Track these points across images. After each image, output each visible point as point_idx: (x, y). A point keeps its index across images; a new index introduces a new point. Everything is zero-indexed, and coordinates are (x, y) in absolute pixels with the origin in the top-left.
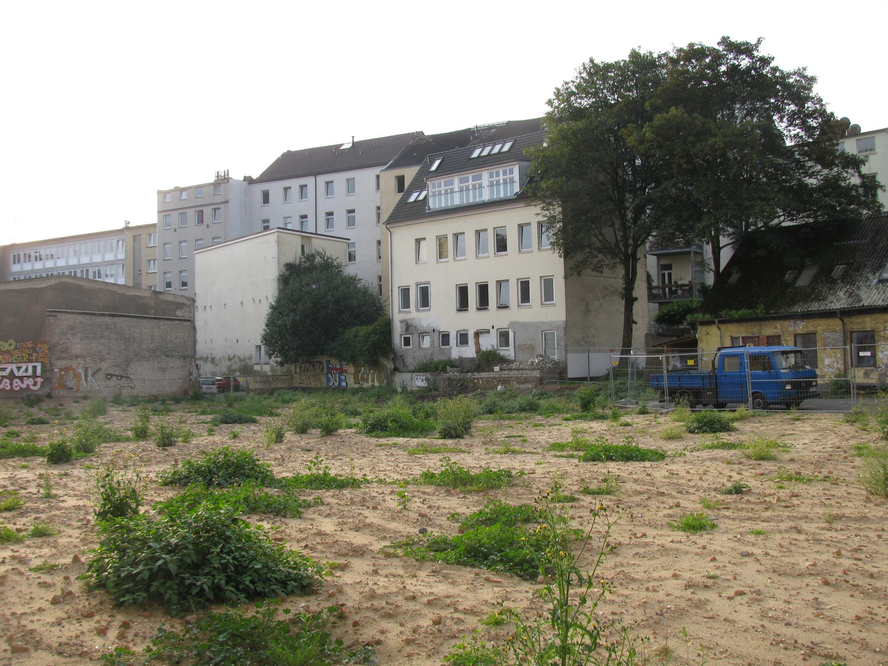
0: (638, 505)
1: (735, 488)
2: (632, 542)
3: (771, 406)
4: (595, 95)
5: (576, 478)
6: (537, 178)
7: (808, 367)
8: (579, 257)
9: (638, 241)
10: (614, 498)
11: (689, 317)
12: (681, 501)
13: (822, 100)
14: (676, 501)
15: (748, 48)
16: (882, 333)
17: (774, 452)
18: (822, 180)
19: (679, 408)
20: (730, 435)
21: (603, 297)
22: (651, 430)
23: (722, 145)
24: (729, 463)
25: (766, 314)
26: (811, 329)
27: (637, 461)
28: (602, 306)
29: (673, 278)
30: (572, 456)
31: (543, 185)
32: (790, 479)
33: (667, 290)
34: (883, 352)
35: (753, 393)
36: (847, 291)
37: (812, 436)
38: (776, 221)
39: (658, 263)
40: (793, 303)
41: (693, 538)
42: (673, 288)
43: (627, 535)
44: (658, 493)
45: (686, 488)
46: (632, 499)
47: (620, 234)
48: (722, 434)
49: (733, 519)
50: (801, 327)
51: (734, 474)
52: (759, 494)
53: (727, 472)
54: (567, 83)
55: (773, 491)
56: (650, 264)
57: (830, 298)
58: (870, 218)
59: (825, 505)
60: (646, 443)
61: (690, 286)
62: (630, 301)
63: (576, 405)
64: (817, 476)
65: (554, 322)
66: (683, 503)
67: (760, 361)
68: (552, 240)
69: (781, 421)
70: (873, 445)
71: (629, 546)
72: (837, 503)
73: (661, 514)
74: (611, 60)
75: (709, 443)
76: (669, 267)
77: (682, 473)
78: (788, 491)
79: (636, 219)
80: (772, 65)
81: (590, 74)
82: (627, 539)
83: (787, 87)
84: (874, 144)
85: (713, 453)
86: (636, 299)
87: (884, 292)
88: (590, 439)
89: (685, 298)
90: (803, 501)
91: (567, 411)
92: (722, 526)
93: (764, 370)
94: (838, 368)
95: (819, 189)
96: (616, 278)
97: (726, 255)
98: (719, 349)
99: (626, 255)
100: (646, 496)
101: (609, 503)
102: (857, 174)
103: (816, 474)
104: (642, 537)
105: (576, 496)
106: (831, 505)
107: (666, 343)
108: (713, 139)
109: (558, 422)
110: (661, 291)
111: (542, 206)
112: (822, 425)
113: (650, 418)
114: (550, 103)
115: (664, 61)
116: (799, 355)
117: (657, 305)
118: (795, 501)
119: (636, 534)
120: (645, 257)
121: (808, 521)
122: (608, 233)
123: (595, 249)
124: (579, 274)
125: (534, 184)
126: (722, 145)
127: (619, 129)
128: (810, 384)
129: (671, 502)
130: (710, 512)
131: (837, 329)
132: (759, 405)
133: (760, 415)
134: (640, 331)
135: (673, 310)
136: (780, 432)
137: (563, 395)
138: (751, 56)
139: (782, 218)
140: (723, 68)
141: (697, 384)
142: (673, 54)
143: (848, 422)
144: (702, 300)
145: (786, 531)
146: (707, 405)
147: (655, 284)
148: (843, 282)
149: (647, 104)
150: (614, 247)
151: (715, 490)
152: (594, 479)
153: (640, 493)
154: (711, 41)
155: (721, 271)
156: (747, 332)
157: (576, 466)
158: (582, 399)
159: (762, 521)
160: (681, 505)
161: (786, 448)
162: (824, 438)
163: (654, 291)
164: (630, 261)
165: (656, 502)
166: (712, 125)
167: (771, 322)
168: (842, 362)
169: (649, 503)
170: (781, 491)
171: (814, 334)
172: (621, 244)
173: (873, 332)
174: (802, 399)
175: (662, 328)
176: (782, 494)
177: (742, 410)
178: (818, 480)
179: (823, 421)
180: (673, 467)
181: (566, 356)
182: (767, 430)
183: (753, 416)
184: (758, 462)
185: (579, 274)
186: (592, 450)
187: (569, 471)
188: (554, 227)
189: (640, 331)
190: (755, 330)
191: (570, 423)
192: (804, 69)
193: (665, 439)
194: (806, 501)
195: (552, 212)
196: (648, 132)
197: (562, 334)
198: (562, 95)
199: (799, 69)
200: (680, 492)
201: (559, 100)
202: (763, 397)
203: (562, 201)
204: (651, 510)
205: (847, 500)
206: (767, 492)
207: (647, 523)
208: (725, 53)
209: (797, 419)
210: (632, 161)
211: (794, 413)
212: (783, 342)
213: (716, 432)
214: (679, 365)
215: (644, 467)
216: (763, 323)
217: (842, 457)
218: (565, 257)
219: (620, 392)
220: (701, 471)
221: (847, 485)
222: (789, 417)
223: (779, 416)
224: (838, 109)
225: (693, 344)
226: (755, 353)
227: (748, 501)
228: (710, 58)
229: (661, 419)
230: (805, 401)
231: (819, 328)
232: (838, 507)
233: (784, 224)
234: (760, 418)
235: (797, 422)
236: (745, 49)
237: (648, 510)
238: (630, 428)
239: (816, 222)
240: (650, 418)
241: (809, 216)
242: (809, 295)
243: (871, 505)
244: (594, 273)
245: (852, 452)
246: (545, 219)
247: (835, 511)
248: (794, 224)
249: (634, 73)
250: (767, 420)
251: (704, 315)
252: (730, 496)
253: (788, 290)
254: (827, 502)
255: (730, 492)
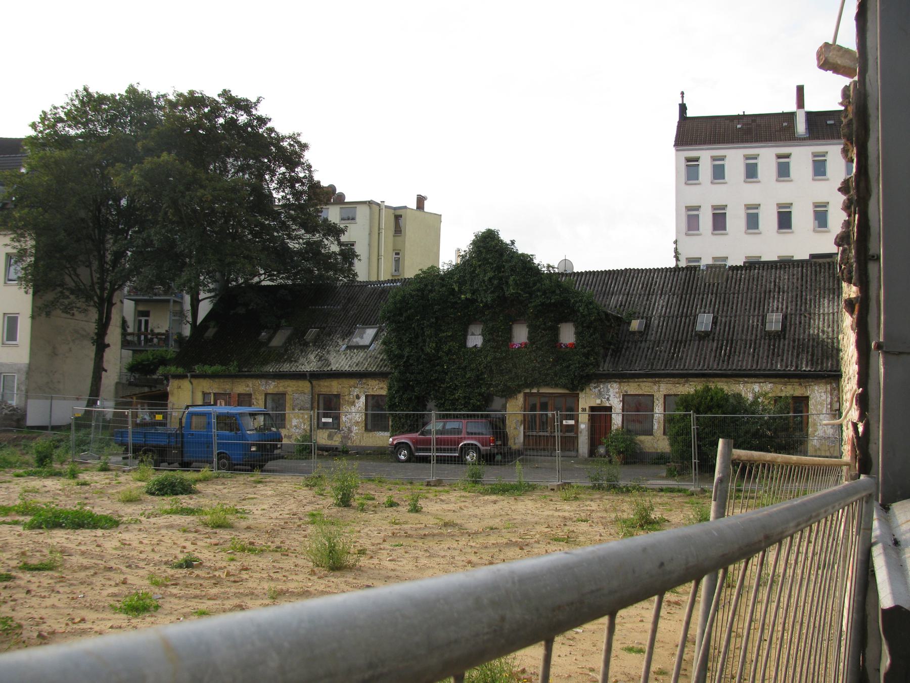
0: (82, 583)
1: (186, 561)
2: (69, 629)
3: (236, 467)
4: (85, 125)
5: (16, 551)
6: (11, 206)
7: (274, 429)
8: (50, 296)
9: (115, 285)
10: (57, 574)
11: (161, 370)
12: (129, 577)
13: (311, 167)
14: (122, 577)
15: (247, 105)
16: (347, 398)
17: (231, 518)
18: (304, 244)
19: (142, 466)
20: (191, 499)
21: (73, 341)
22: (110, 491)
23: (210, 198)
24: (185, 531)
25: (239, 371)
26: (281, 389)
27: (88, 528)
28: (70, 350)
29: (150, 325)
30: (16, 523)
31: (17, 215)
32: (243, 550)
33: (143, 337)
34: (346, 415)
35: (218, 454)
36: (317, 354)
37: (272, 501)
38: (256, 279)
39: (135, 309)
40: (266, 362)
41: (134, 621)
42: (149, 336)
43: (64, 620)
44: (105, 567)
45: (136, 561)
46: (76, 575)
47: (96, 276)
48: (184, 496)
49: (180, 598)
50: (272, 387)
51: (188, 544)
52: (210, 567)
53: (182, 542)
54: (55, 108)
55: (224, 564)
56: (126, 308)
57: (302, 360)
58: (344, 285)
59: (272, 579)
60: (101, 508)
61: (167, 334)
62: (101, 346)
63: (31, 458)
64: (270, 547)
65: (15, 364)
66: (131, 579)
67: (228, 422)
68: (20, 275)
69: (244, 484)
70: (326, 511)
71: (64, 635)
72: (284, 576)
73: (105, 593)
74: (107, 92)
75: (168, 507)
76: (146, 314)
77: (135, 544)
78: (239, 564)
79: (115, 262)
80: (269, 125)
81: (82, 102)
82: (63, 626)
83: (281, 149)
84: (355, 213)
85: (171, 519)
86: (108, 345)
87: (351, 358)
88: (41, 501)
89: (161, 347)
90: (252, 574)
91: (20, 467)
92: (167, 606)
93: (231, 430)
94: (304, 429)
95: (299, 253)
96: (89, 322)
97: (205, 308)
98: (187, 407)
99: (101, 299)
100: (92, 572)
101: (50, 581)
102: (336, 242)
103: (269, 544)
104: (80, 622)
105: (14, 573)
106: (278, 579)
107: (135, 395)
108: (202, 191)
109: (8, 479)
110: (136, 339)
111: (12, 236)
112: (284, 490)
113: (111, 476)
114: (34, 126)
115: (162, 103)
116: (267, 416)
117: (131, 352)
118: (244, 575)
119: (73, 619)
120: (122, 302)
121: (253, 597)
122: (84, 272)
123: (67, 289)
124: (48, 314)
125: (6, 212)
126: (210, 198)
127: (107, 165)
128: (275, 447)
129: (119, 578)
130: (157, 590)
131: (306, 391)
132: (224, 465)
133: (223, 477)
134: (110, 379)
135: (148, 360)
136: (241, 495)
137: (20, 445)
138: (249, 113)
139: (262, 277)
140: (221, 121)
141: (163, 442)
142: (172, 97)
143: (307, 486)
144: (178, 350)
145: (231, 610)
146: (172, 463)
147: (130, 330)
148: (314, 345)
149: (139, 145)
150: (88, 288)
151: (166, 563)
152: (37, 551)
153: (86, 568)
154: (212, 92)
155: (198, 324)
156: (218, 388)
157: (20, 535)
158: (38, 452)
159: (209, 599)
160: (129, 582)
161: (242, 514)
162: (283, 503)
163: (129, 338)
164: (105, 305)
165: (102, 579)
166: (202, 175)
167: (243, 380)
168: (309, 423)
169: (94, 580)
170: (232, 564)
171: (283, 395)
172: (97, 287)
173: (338, 396)
174: (267, 461)
175: (134, 376)
176: (233, 567)
177: (206, 471)
178: (270, 551)
179: (285, 485)
180: (126, 536)
181: (26, 402)
182: (229, 492)
183: (217, 477)
184: (215, 530)
185: (48, 314)
186: (40, 516)
187: (10, 541)
188: (23, 261)
189: (110, 379)
190: (227, 386)
191: (22, 480)
192: (299, 135)
193: (124, 501)
194: (254, 575)
195: (24, 245)
196: (135, 174)
197: (23, 377)
198: (49, 120)
199: (294, 134)
200: (129, 566)
201: (44, 125)
202: (228, 459)
203: (36, 233)
204: (96, 588)
205: (293, 573)
206: (219, 565)
207: (88, 605)
208: (224, 105)
209: (260, 482)
210: (117, 200)
211: (258, 475)
212: (254, 401)
213: (177, 494)
214: (147, 418)
215: (96, 536)
216: (235, 380)
217: (296, 526)
218: (34, 294)
219: (81, 444)
220: (155, 541)
221: (296, 556)
222: (253, 479)
223: (242, 478)
224: (323, 178)
225: (164, 397)
226: (223, 414)
227: (198, 576)
228: (209, 108)
229: (123, 478)
230: (269, 463)
231: (289, 389)
232: (284, 581)
233: (263, 283)
234: (223, 480)
235: (259, 485)
236: (244, 106)
237: (92, 588)
238: (88, 487)
239: (294, 284)
240: (111, 476)
241: (288, 278)
242: (283, 355)
243: (315, 578)
244: (65, 315)
245: (307, 519)
246: (15, 251)
247: (281, 586)
248: (274, 284)
249: (130, 109)
250: (229, 483)
251: (177, 368)
252: (180, 571)
253: (263, 349)
254: (274, 576)
255: (180, 566)
